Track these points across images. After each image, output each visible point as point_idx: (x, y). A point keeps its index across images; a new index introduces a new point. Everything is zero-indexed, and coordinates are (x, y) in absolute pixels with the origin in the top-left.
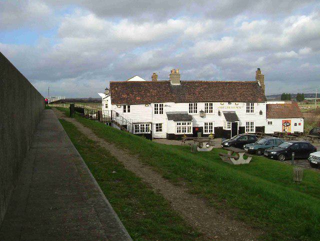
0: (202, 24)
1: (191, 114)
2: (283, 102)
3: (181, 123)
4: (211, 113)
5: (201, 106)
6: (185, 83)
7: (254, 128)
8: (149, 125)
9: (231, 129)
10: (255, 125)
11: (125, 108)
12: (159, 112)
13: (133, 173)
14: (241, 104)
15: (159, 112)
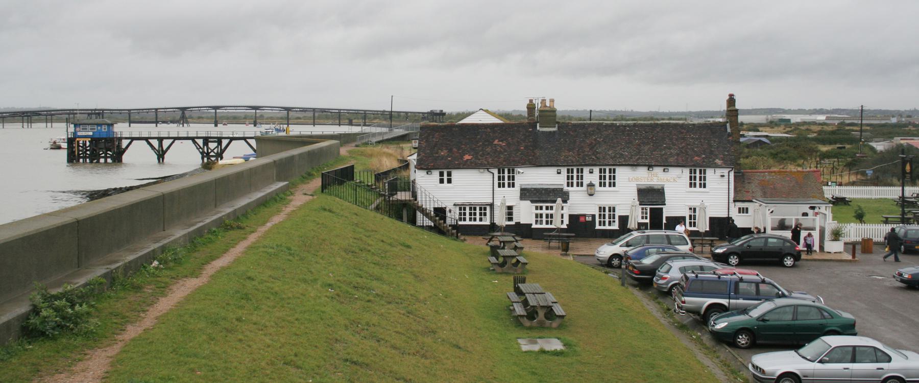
0: (104, 280)
1: (570, 189)
2: (895, 162)
3: (544, 205)
4: (612, 188)
5: (591, 176)
6: (567, 125)
7: (617, 219)
8: (485, 209)
9: (648, 221)
10: (617, 214)
11: (441, 174)
12: (506, 185)
13: (216, 206)
14: (674, 172)
15: (506, 185)
